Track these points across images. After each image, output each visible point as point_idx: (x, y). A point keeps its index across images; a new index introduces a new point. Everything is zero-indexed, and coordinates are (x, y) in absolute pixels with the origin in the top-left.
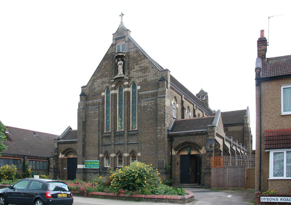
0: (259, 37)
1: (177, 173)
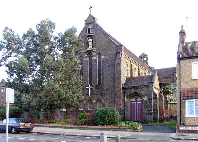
0: (180, 30)
1: (128, 113)
